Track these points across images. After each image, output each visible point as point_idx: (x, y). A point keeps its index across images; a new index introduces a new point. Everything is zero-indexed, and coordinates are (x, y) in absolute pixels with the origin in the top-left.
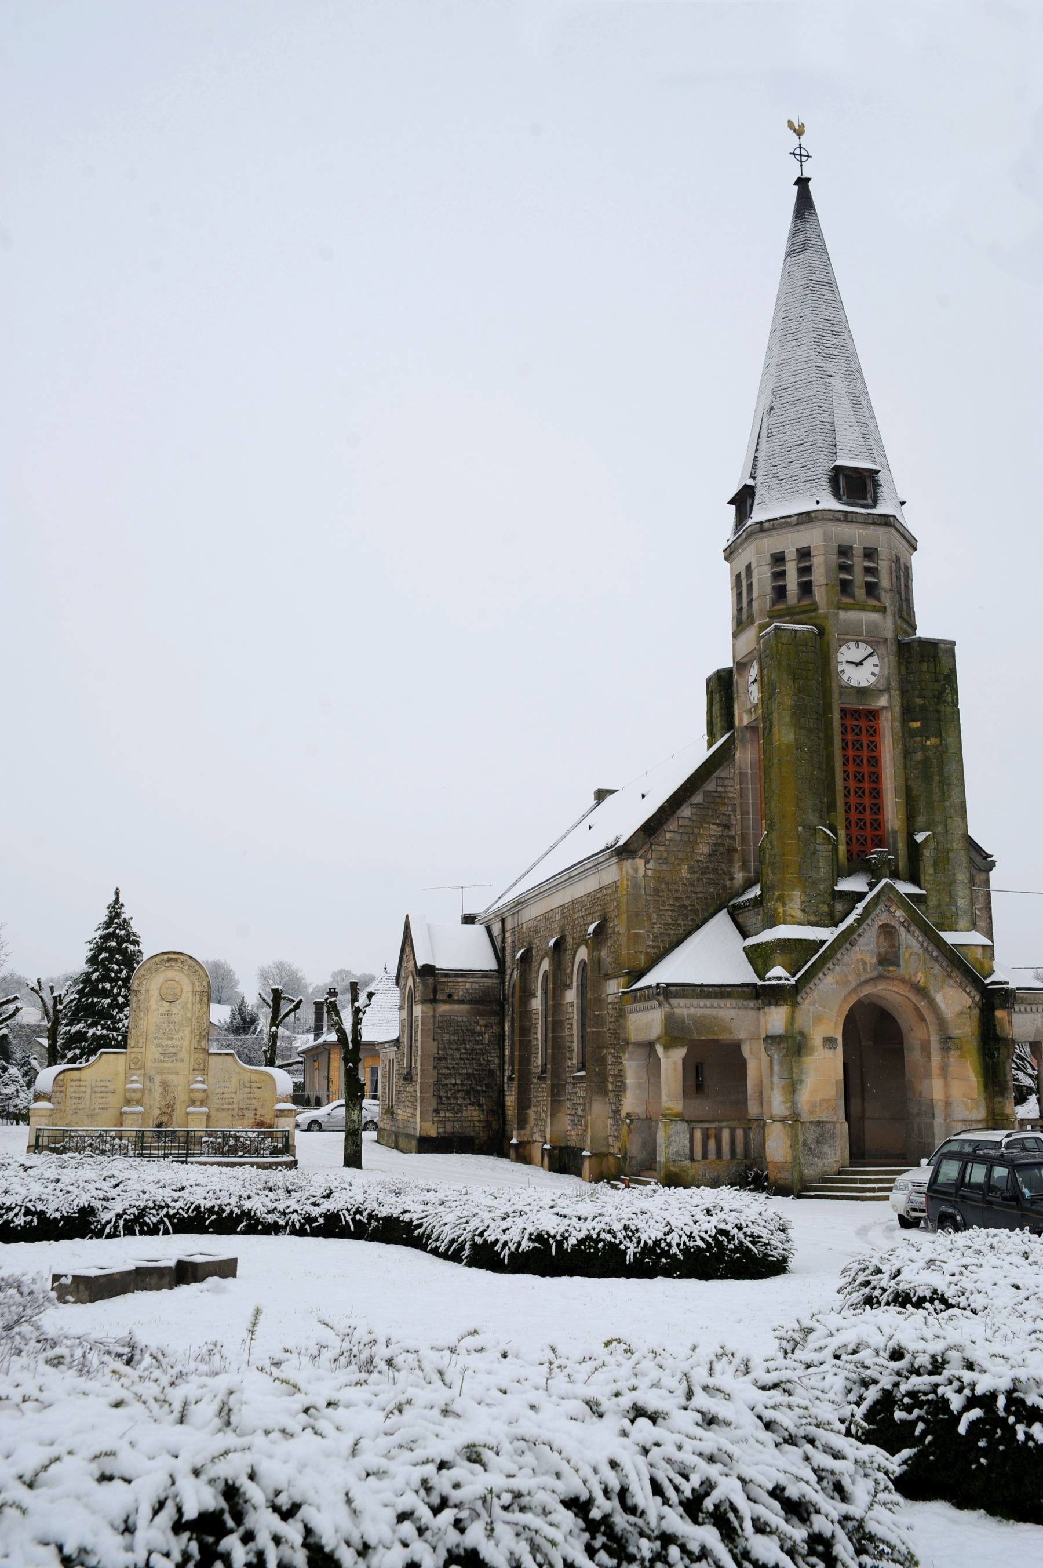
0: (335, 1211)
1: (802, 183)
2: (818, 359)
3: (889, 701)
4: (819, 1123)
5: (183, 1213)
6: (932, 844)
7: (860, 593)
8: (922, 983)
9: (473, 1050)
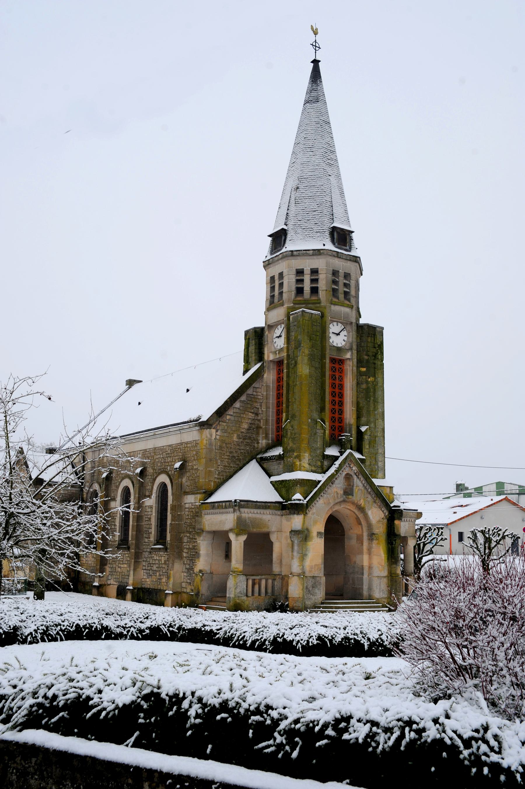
0: (156, 626)
1: (316, 62)
2: (324, 165)
3: (352, 355)
4: (313, 577)
5: (70, 628)
6: (369, 433)
7: (341, 296)
8: (362, 505)
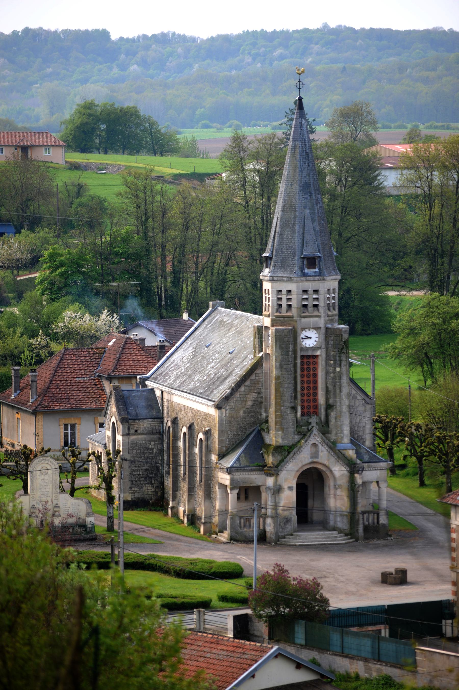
3: (321, 352)
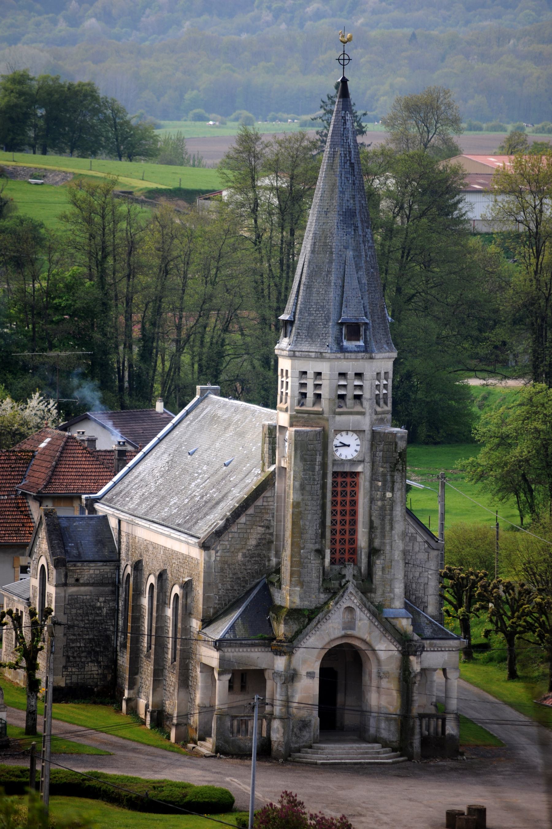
3: (364, 468)
9: (94, 620)
